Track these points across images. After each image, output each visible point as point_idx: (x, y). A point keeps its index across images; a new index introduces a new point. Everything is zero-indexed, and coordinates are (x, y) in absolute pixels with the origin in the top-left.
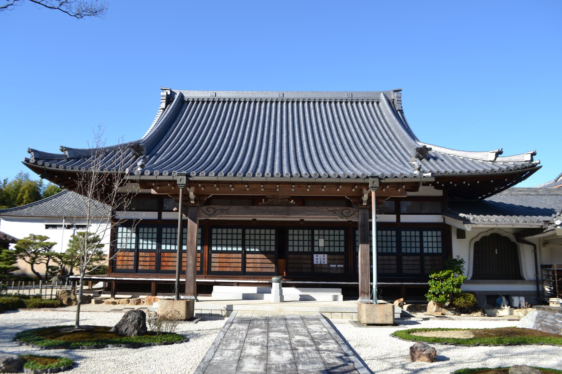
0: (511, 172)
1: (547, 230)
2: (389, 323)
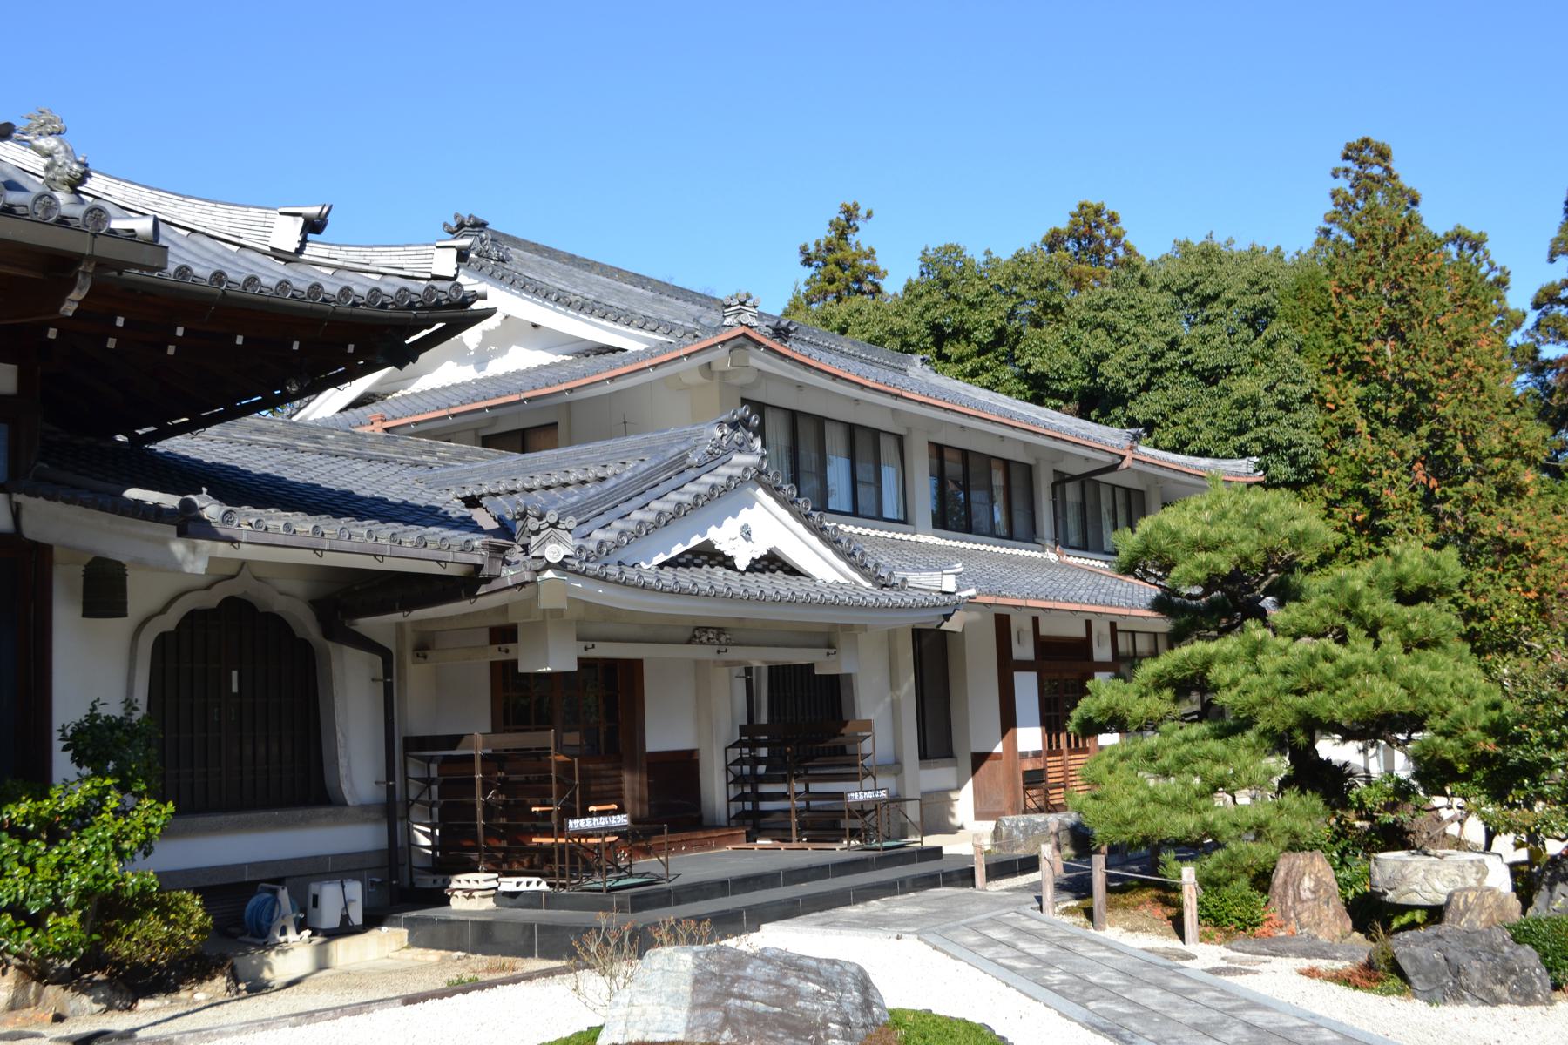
1: (496, 584)
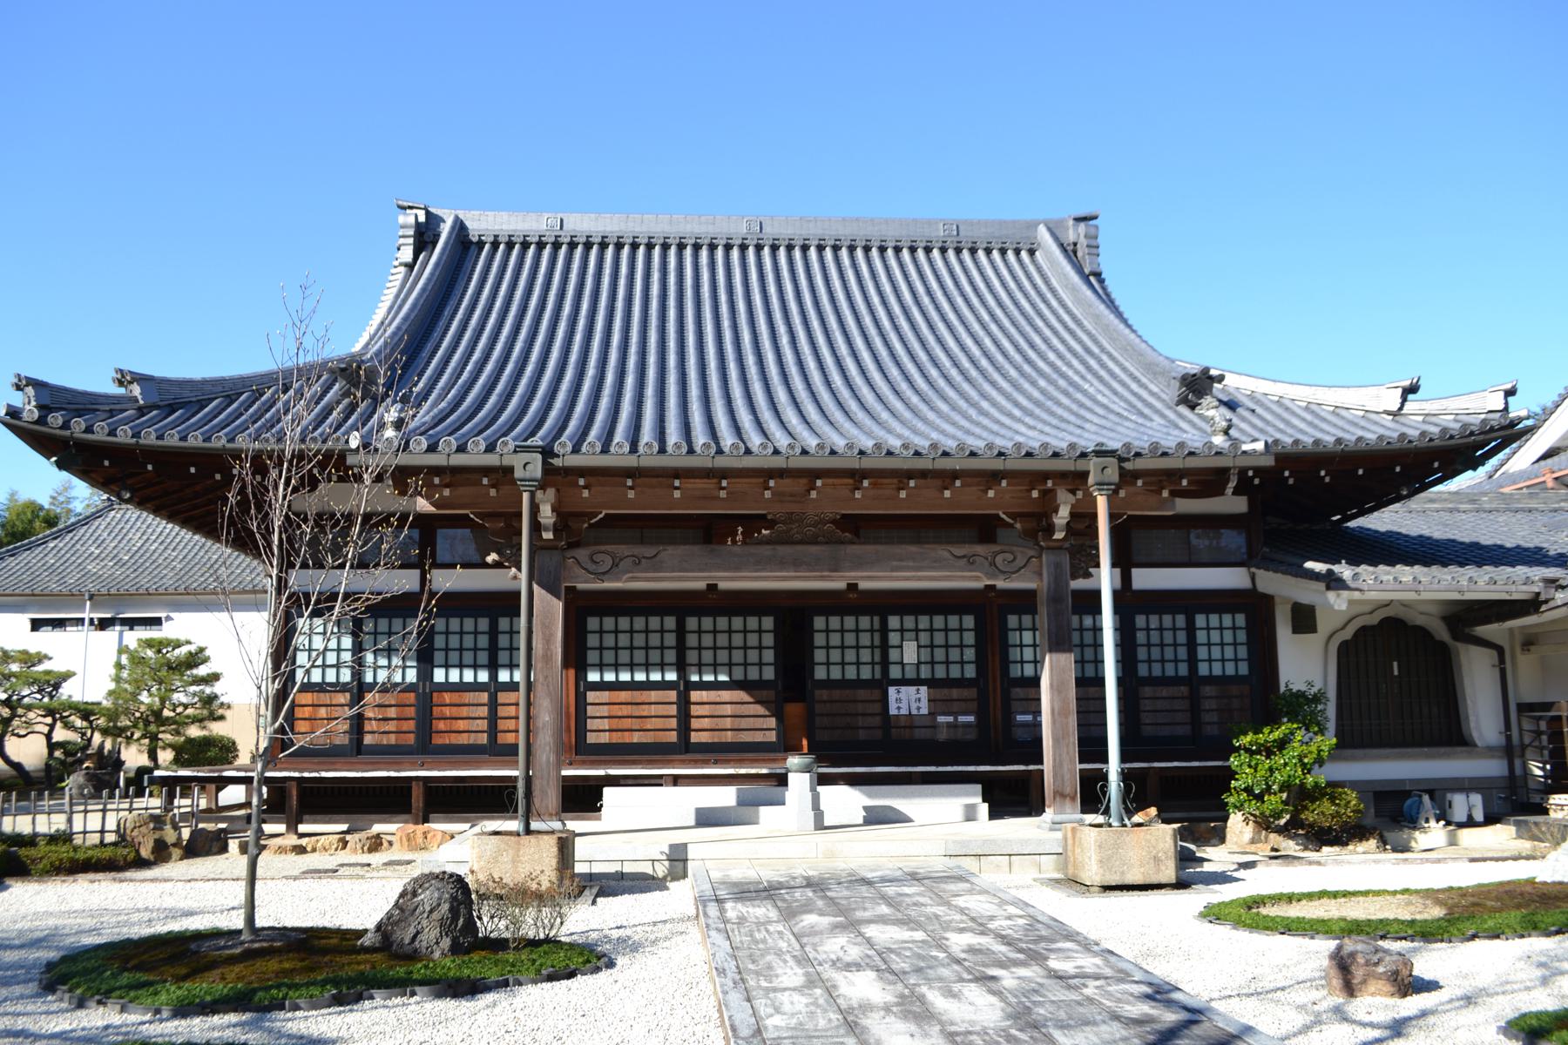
0: (1452, 442)
1: (1551, 604)
2: (1164, 881)
